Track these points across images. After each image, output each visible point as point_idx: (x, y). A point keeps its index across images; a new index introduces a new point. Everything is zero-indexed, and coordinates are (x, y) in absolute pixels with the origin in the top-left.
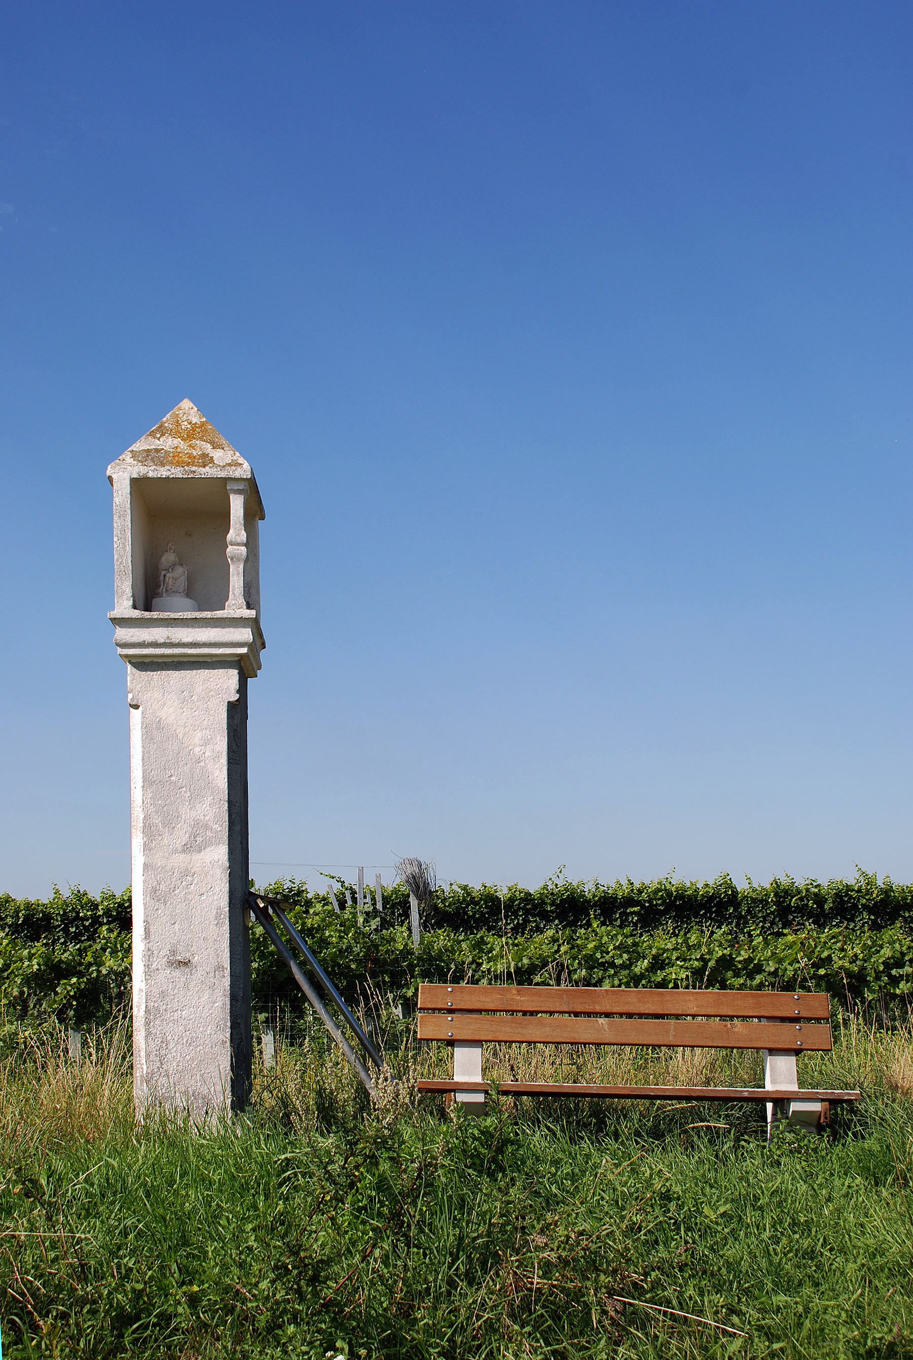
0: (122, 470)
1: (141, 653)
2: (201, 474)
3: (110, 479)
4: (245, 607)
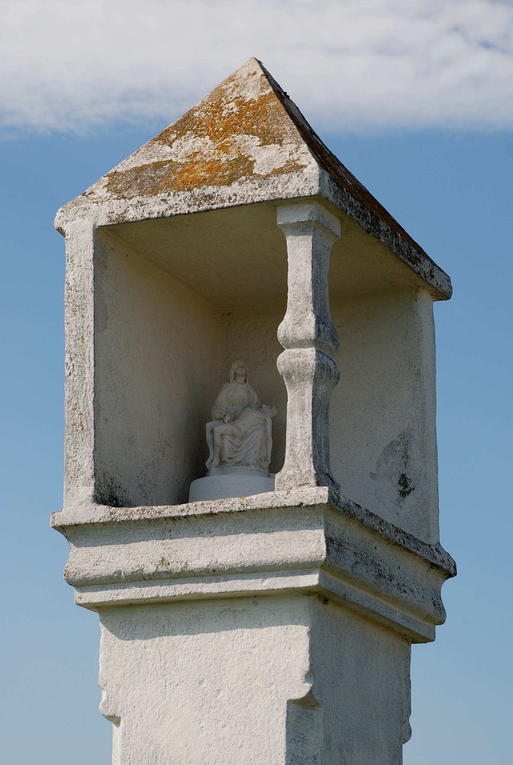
0: (81, 213)
1: (116, 598)
2: (223, 201)
3: (60, 230)
4: (313, 481)
